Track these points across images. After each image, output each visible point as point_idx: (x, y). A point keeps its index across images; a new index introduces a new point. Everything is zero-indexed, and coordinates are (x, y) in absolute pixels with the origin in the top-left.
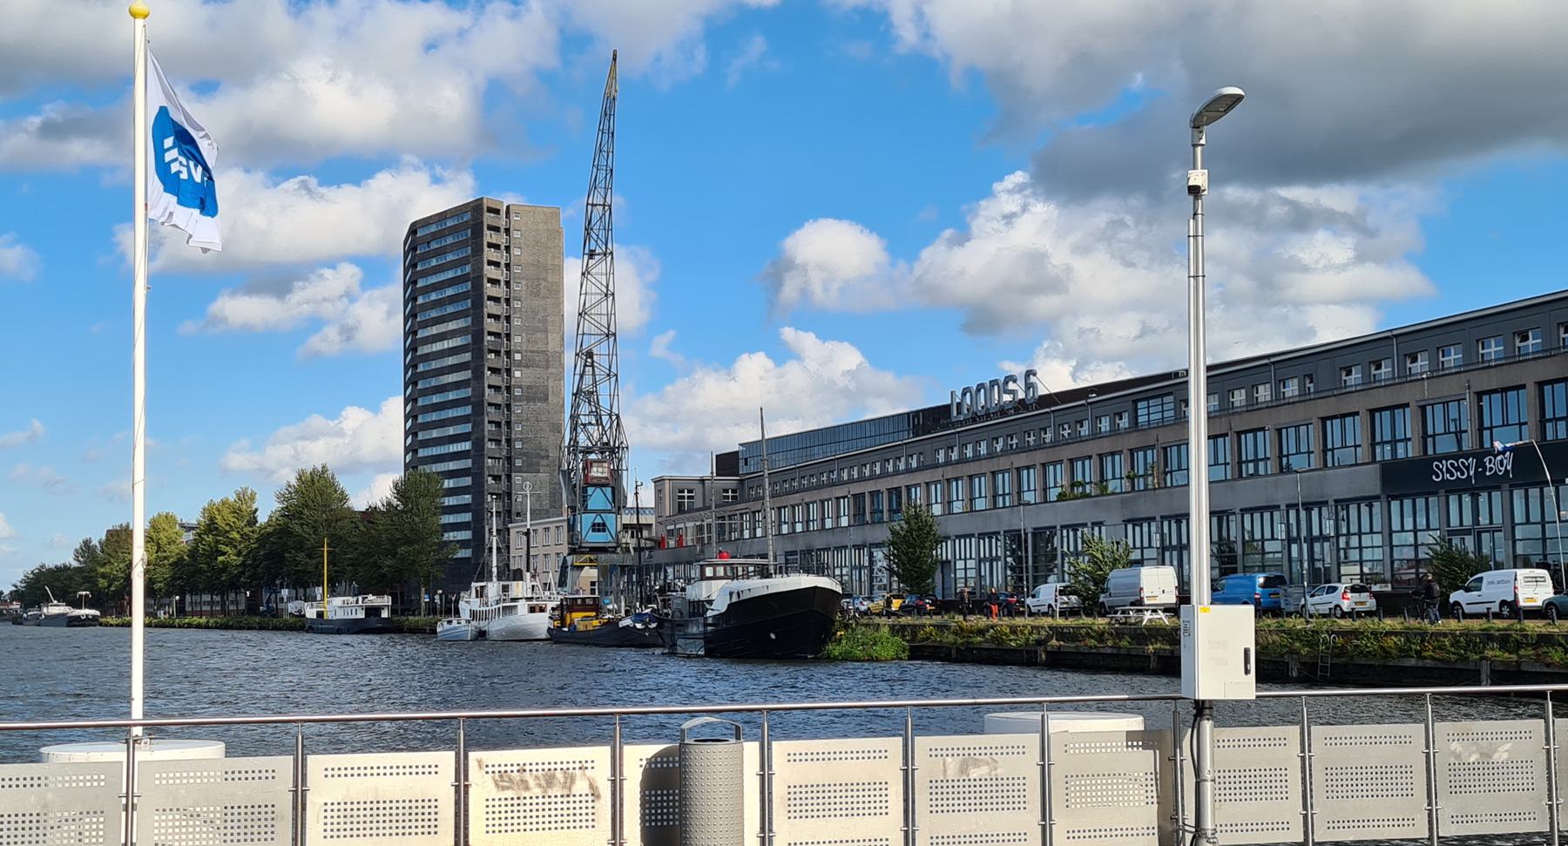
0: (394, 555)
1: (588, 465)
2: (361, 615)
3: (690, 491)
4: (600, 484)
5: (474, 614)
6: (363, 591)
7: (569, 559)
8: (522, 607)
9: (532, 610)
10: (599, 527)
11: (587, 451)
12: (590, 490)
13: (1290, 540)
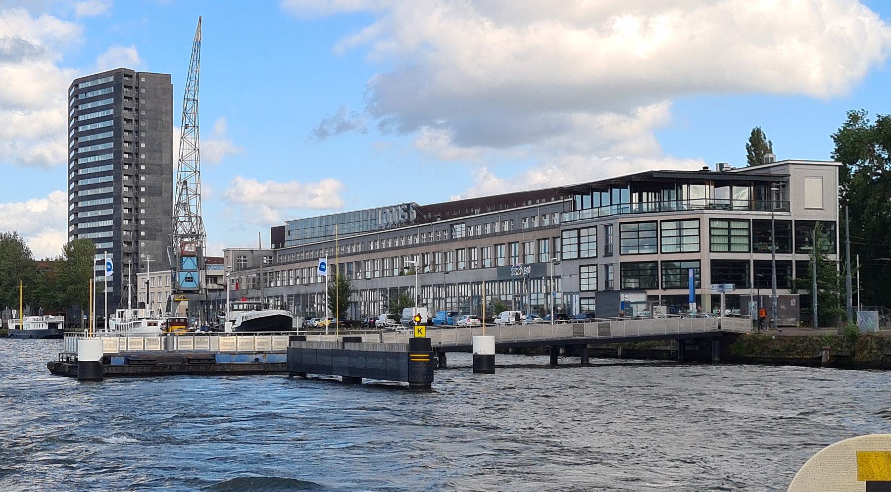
0: (64, 291)
1: (183, 244)
2: (46, 327)
3: (245, 257)
4: (190, 255)
5: (117, 327)
6: (46, 313)
7: (172, 297)
8: (144, 322)
9: (150, 324)
10: (189, 279)
11: (182, 237)
12: (184, 259)
13: (434, 299)
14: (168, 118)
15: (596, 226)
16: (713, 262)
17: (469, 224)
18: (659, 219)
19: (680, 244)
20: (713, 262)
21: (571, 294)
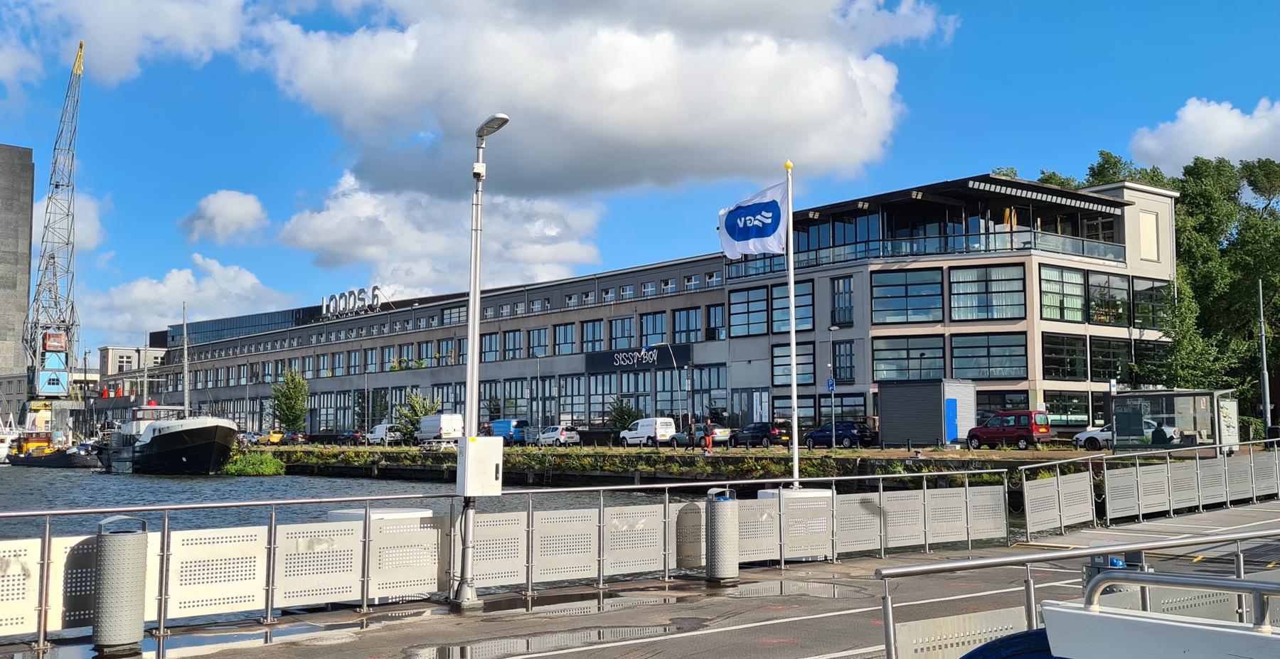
13: (532, 399)
14: (27, 199)
15: (812, 281)
16: (1047, 338)
17: (418, 315)
18: (945, 265)
19: (987, 306)
20: (1047, 338)
21: (750, 391)
